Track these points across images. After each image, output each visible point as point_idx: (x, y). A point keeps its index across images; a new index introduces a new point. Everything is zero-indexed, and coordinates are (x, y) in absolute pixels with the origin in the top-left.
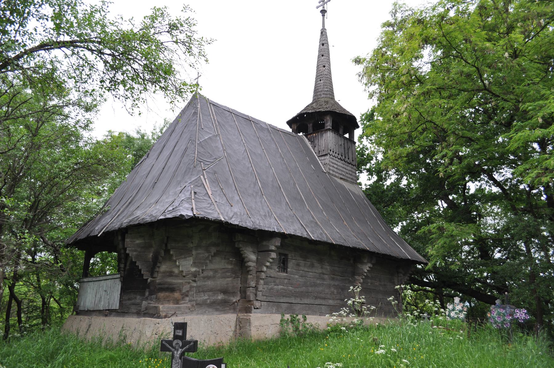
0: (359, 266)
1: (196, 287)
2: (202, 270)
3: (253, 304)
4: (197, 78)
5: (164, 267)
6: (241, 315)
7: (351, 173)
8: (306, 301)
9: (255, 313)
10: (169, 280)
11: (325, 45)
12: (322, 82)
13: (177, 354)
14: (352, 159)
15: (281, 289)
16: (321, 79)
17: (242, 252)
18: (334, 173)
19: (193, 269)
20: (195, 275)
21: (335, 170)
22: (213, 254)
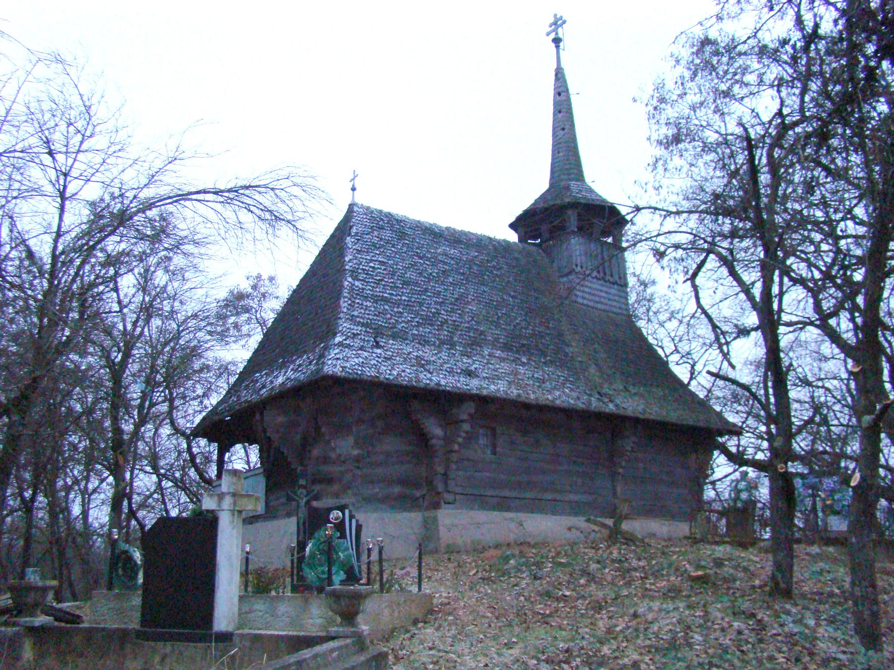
0: (619, 442)
2: (368, 452)
4: (353, 179)
5: (316, 452)
6: (427, 514)
7: (617, 298)
8: (529, 495)
9: (445, 508)
10: (324, 468)
11: (563, 94)
12: (561, 154)
18: (585, 302)
19: (355, 452)
20: (358, 459)
21: (587, 296)
22: (379, 429)
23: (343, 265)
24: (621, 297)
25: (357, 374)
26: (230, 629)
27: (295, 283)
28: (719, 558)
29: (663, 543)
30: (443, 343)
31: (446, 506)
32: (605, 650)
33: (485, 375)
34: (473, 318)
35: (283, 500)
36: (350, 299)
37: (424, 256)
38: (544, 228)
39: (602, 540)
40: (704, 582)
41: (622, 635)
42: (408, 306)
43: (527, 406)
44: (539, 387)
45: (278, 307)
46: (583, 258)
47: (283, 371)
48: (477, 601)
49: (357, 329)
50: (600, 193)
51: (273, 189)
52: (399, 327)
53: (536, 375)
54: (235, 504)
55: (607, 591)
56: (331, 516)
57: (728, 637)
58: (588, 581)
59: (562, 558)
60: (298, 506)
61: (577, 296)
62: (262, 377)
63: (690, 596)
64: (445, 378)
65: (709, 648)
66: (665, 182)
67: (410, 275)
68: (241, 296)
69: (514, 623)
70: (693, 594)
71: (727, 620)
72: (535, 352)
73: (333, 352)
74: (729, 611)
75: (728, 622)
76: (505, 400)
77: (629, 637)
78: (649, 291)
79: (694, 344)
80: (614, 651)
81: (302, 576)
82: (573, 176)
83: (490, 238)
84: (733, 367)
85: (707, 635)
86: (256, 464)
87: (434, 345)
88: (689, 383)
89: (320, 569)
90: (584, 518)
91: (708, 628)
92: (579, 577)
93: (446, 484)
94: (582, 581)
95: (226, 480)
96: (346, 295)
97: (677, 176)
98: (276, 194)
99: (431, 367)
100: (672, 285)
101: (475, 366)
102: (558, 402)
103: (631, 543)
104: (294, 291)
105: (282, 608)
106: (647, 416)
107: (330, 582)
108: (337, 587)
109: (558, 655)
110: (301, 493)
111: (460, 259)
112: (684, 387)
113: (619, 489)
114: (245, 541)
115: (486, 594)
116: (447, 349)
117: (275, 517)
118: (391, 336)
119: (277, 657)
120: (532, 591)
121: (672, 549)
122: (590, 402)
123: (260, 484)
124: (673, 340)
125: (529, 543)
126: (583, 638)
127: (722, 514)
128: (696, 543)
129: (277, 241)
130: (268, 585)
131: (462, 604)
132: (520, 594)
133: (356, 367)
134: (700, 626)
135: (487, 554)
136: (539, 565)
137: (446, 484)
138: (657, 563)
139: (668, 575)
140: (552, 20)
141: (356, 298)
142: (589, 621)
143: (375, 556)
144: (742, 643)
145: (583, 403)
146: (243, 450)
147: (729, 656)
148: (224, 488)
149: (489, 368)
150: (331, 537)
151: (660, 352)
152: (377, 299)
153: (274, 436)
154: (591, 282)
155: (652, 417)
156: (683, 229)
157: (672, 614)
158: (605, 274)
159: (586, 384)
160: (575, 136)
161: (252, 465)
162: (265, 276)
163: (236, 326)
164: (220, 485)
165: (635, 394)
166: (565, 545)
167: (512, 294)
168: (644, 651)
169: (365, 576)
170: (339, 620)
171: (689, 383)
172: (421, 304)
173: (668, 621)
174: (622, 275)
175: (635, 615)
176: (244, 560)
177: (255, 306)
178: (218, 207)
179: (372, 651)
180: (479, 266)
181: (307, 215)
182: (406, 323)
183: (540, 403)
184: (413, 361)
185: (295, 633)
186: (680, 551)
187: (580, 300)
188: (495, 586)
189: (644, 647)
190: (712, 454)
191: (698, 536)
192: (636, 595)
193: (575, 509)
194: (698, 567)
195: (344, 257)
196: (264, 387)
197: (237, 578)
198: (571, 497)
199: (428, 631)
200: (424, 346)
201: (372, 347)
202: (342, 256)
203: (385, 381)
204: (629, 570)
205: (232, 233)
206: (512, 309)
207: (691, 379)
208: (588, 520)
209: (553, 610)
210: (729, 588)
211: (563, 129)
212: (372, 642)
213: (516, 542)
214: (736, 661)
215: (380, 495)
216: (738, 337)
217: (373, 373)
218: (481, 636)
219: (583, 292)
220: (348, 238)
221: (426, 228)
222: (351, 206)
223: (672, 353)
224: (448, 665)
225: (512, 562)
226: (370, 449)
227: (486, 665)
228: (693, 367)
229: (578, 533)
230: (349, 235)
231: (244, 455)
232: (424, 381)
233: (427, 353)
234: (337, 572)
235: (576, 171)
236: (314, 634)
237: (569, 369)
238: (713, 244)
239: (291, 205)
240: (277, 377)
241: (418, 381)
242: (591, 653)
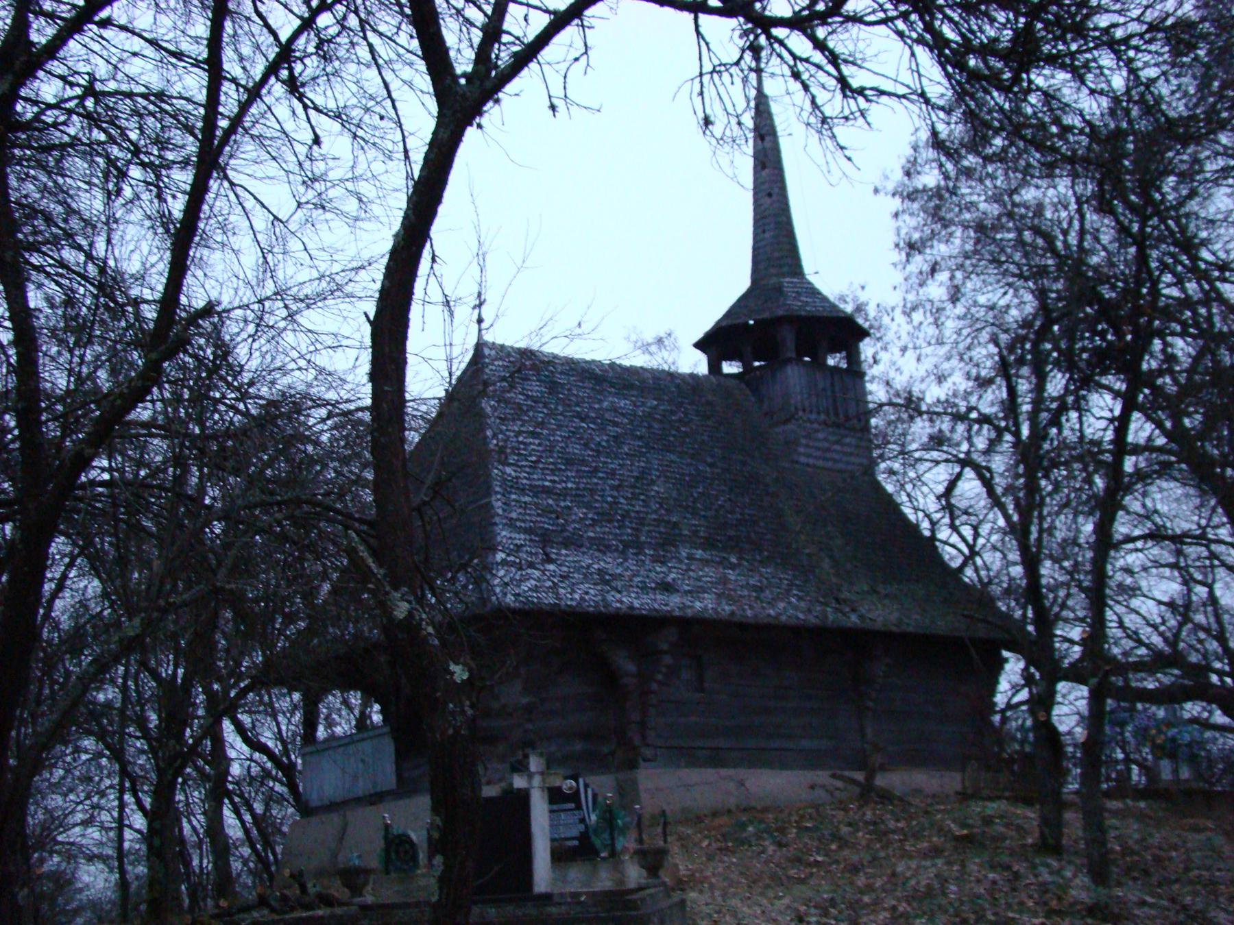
11: (768, 139)
12: (767, 235)
16: (767, 228)
18: (811, 461)
26: (549, 890)
29: (929, 801)
30: (627, 545)
31: (647, 764)
33: (687, 588)
34: (661, 504)
40: (971, 842)
42: (577, 497)
43: (743, 626)
44: (757, 598)
49: (520, 538)
54: (544, 781)
67: (575, 449)
72: (747, 546)
76: (715, 620)
82: (785, 269)
87: (616, 550)
93: (644, 737)
94: (833, 847)
96: (498, 489)
99: (619, 584)
101: (673, 576)
102: (783, 618)
111: (635, 415)
122: (825, 612)
125: (754, 808)
134: (957, 878)
136: (782, 830)
141: (510, 493)
145: (817, 617)
149: (689, 578)
155: (910, 629)
165: (887, 596)
167: (709, 460)
175: (894, 874)
180: (661, 422)
184: (596, 577)
187: (803, 459)
193: (811, 760)
194: (963, 825)
198: (806, 743)
208: (834, 776)
211: (770, 195)
213: (738, 807)
221: (584, 371)
222: (480, 346)
225: (750, 829)
233: (609, 563)
235: (789, 261)
241: (607, 605)
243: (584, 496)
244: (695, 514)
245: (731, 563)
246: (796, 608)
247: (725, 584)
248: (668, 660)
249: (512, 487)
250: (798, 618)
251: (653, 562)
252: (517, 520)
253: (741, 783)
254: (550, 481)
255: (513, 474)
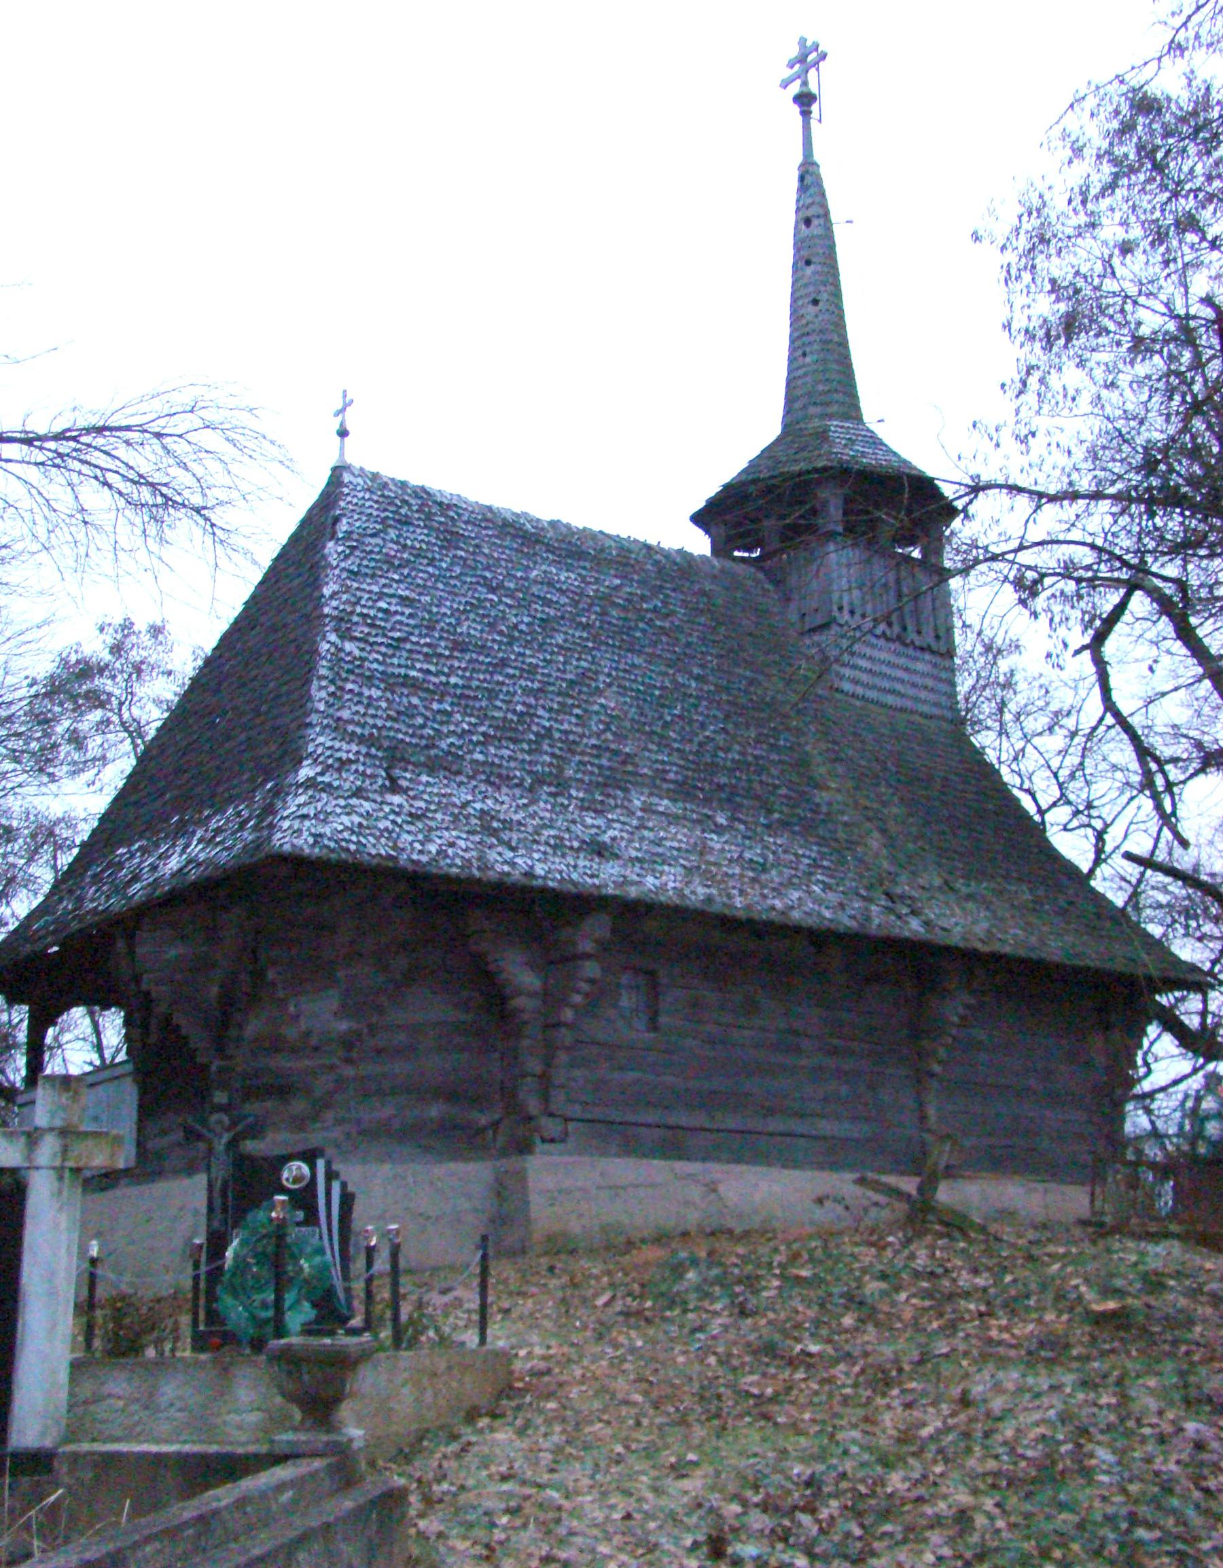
1: (355, 1079)
3: (537, 1129)
4: (343, 410)
5: (254, 1026)
7: (930, 683)
9: (544, 1153)
11: (815, 222)
12: (808, 359)
13: (220, 1144)
14: (932, 634)
15: (636, 1082)
16: (808, 350)
17: (492, 967)
18: (860, 691)
19: (344, 1026)
20: (348, 1042)
21: (864, 677)
23: (319, 606)
24: (941, 680)
25: (348, 850)
26: (48, 1443)
27: (209, 642)
28: (1156, 1273)
29: (1031, 1234)
30: (540, 781)
31: (547, 1146)
32: (896, 1481)
33: (634, 854)
34: (608, 725)
35: (179, 1135)
36: (332, 682)
37: (501, 586)
38: (770, 525)
39: (892, 1227)
41: (933, 1447)
42: (463, 699)
43: (728, 923)
45: (170, 696)
46: (856, 593)
47: (181, 842)
48: (612, 1365)
49: (348, 750)
50: (894, 447)
51: (158, 435)
52: (443, 745)
53: (747, 855)
54: (65, 1150)
55: (901, 1344)
56: (285, 1174)
57: (1174, 1457)
58: (861, 1320)
59: (802, 1266)
60: (210, 1151)
61: (841, 678)
62: (132, 856)
63: (1088, 1358)
64: (545, 861)
65: (1130, 1481)
66: (1041, 423)
67: (470, 628)
68: (86, 670)
69: (691, 1418)
70: (1095, 1352)
71: (1170, 1415)
73: (295, 802)
74: (1177, 1397)
75: (1173, 1422)
77: (950, 1451)
78: (1004, 665)
79: (1099, 788)
80: (916, 1483)
81: (216, 1312)
82: (834, 409)
83: (649, 548)
84: (1184, 844)
85: (1123, 1452)
86: (118, 1051)
88: (1092, 871)
89: (258, 1297)
90: (856, 1175)
91: (1129, 1434)
92: (839, 1310)
93: (546, 1099)
94: (848, 1321)
95: (43, 1096)
96: (323, 672)
97: (1066, 412)
98: (164, 447)
100: (1054, 652)
101: (611, 833)
102: (796, 915)
103: (957, 1234)
104: (208, 662)
105: (169, 1390)
106: (996, 947)
107: (280, 1331)
108: (295, 1340)
109: (789, 1492)
110: (220, 1122)
111: (581, 594)
112: (1079, 880)
113: (931, 1112)
114: (87, 1230)
115: (633, 1350)
116: (551, 794)
117: (157, 1174)
118: (424, 765)
119: (155, 1507)
120: (735, 1343)
121: (1051, 1248)
123: (128, 1095)
124: (1055, 775)
125: (730, 1232)
126: (846, 1452)
127: (1165, 1170)
128: (1103, 1235)
129: (167, 553)
130: (138, 1335)
131: (578, 1372)
132: (706, 1351)
133: (346, 835)
134: (1110, 1428)
135: (635, 1257)
136: (751, 1282)
137: (546, 1099)
138: (1015, 1281)
139: (1041, 1309)
140: (794, 52)
141: (346, 680)
142: (861, 1412)
143: (382, 1264)
144: (1206, 1471)
145: (853, 917)
146: (87, 1021)
147: (1175, 1502)
148: (41, 1117)
149: (642, 839)
150: (282, 1224)
151: (1027, 803)
152: (392, 683)
153: (162, 992)
154: (873, 646)
155: (1007, 949)
156: (1075, 535)
157: (1045, 1400)
158: (904, 629)
159: (861, 876)
160: (841, 317)
161: (108, 1054)
162: (141, 625)
163: (77, 740)
164: (33, 1102)
165: (969, 897)
166: (811, 1237)
167: (696, 671)
168: (982, 1487)
169: (359, 1305)
170: (297, 1415)
171: (1092, 871)
172: (492, 694)
173: (1037, 1416)
174: (942, 633)
175: (965, 1401)
176: (86, 1281)
177: (117, 692)
178: (33, 474)
179: (372, 1486)
180: (624, 609)
181: (235, 495)
182: (460, 736)
183: (756, 916)
184: (474, 821)
185: (196, 1448)
186: (1065, 1255)
187: (847, 686)
188: (651, 1332)
189: (985, 1475)
190: (1143, 1033)
191: (1108, 1219)
192: (966, 1354)
194: (1107, 1291)
195: (319, 587)
196: (136, 878)
197: (68, 1322)
198: (825, 1127)
199: (500, 1436)
200: (499, 788)
201: (383, 790)
202: (316, 584)
203: (410, 867)
204: (951, 1297)
205: (62, 535)
206: (696, 706)
207: (1097, 861)
208: (861, 1181)
209: (780, 1386)
210: (1175, 1343)
211: (815, 302)
212: (372, 1463)
214: (1190, 1512)
215: (396, 1125)
216: (1202, 770)
217: (383, 848)
218: (619, 1448)
219: (854, 667)
220: (331, 544)
221: (506, 524)
223: (1054, 804)
224: (542, 1516)
226: (374, 1020)
227: (628, 1516)
228: (1100, 836)
229: (840, 1209)
230: (333, 536)
231: (89, 1030)
232: (498, 868)
233: (505, 804)
234: (298, 1302)
236: (240, 1450)
237: (822, 842)
238: (1141, 569)
239: (199, 471)
240: (165, 856)
241: (485, 867)
242: (862, 1489)
243: (476, 698)
244: (664, 743)
245: (716, 824)
246: (818, 901)
247: (701, 854)
248: (591, 969)
249: (350, 671)
250: (819, 915)
251: (582, 809)
252: (351, 721)
253: (712, 1188)
254: (421, 670)
255: (357, 653)
